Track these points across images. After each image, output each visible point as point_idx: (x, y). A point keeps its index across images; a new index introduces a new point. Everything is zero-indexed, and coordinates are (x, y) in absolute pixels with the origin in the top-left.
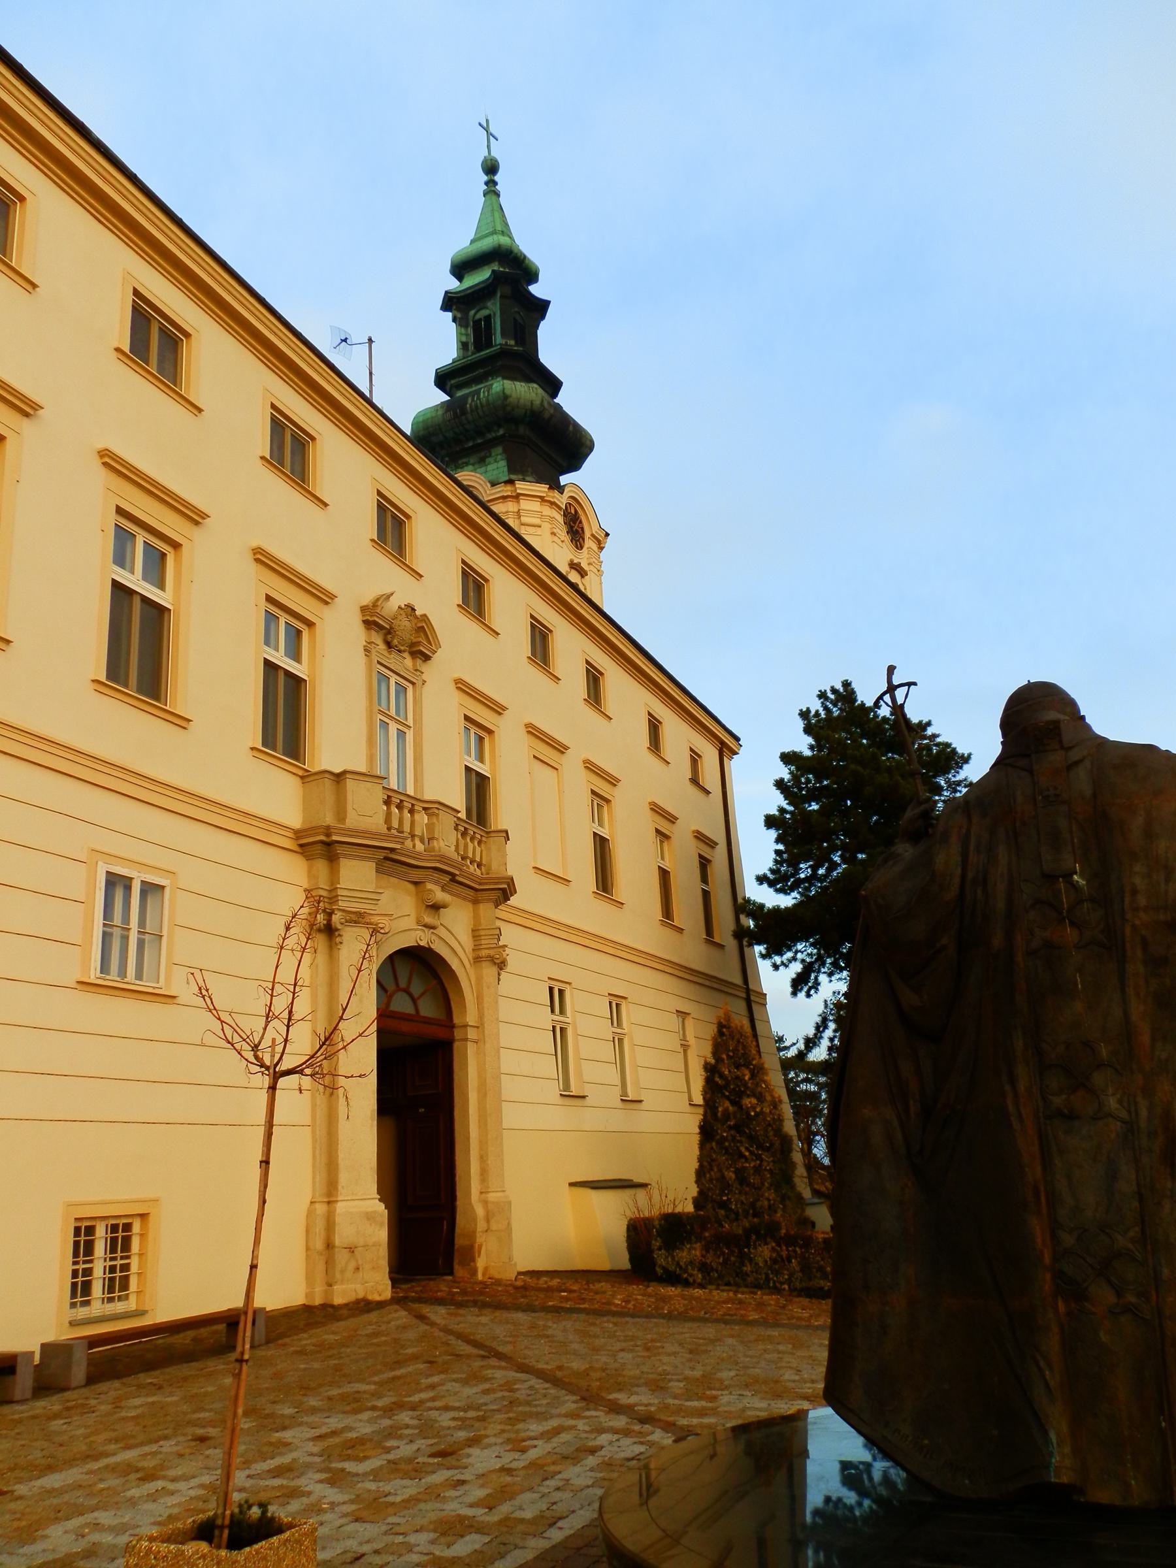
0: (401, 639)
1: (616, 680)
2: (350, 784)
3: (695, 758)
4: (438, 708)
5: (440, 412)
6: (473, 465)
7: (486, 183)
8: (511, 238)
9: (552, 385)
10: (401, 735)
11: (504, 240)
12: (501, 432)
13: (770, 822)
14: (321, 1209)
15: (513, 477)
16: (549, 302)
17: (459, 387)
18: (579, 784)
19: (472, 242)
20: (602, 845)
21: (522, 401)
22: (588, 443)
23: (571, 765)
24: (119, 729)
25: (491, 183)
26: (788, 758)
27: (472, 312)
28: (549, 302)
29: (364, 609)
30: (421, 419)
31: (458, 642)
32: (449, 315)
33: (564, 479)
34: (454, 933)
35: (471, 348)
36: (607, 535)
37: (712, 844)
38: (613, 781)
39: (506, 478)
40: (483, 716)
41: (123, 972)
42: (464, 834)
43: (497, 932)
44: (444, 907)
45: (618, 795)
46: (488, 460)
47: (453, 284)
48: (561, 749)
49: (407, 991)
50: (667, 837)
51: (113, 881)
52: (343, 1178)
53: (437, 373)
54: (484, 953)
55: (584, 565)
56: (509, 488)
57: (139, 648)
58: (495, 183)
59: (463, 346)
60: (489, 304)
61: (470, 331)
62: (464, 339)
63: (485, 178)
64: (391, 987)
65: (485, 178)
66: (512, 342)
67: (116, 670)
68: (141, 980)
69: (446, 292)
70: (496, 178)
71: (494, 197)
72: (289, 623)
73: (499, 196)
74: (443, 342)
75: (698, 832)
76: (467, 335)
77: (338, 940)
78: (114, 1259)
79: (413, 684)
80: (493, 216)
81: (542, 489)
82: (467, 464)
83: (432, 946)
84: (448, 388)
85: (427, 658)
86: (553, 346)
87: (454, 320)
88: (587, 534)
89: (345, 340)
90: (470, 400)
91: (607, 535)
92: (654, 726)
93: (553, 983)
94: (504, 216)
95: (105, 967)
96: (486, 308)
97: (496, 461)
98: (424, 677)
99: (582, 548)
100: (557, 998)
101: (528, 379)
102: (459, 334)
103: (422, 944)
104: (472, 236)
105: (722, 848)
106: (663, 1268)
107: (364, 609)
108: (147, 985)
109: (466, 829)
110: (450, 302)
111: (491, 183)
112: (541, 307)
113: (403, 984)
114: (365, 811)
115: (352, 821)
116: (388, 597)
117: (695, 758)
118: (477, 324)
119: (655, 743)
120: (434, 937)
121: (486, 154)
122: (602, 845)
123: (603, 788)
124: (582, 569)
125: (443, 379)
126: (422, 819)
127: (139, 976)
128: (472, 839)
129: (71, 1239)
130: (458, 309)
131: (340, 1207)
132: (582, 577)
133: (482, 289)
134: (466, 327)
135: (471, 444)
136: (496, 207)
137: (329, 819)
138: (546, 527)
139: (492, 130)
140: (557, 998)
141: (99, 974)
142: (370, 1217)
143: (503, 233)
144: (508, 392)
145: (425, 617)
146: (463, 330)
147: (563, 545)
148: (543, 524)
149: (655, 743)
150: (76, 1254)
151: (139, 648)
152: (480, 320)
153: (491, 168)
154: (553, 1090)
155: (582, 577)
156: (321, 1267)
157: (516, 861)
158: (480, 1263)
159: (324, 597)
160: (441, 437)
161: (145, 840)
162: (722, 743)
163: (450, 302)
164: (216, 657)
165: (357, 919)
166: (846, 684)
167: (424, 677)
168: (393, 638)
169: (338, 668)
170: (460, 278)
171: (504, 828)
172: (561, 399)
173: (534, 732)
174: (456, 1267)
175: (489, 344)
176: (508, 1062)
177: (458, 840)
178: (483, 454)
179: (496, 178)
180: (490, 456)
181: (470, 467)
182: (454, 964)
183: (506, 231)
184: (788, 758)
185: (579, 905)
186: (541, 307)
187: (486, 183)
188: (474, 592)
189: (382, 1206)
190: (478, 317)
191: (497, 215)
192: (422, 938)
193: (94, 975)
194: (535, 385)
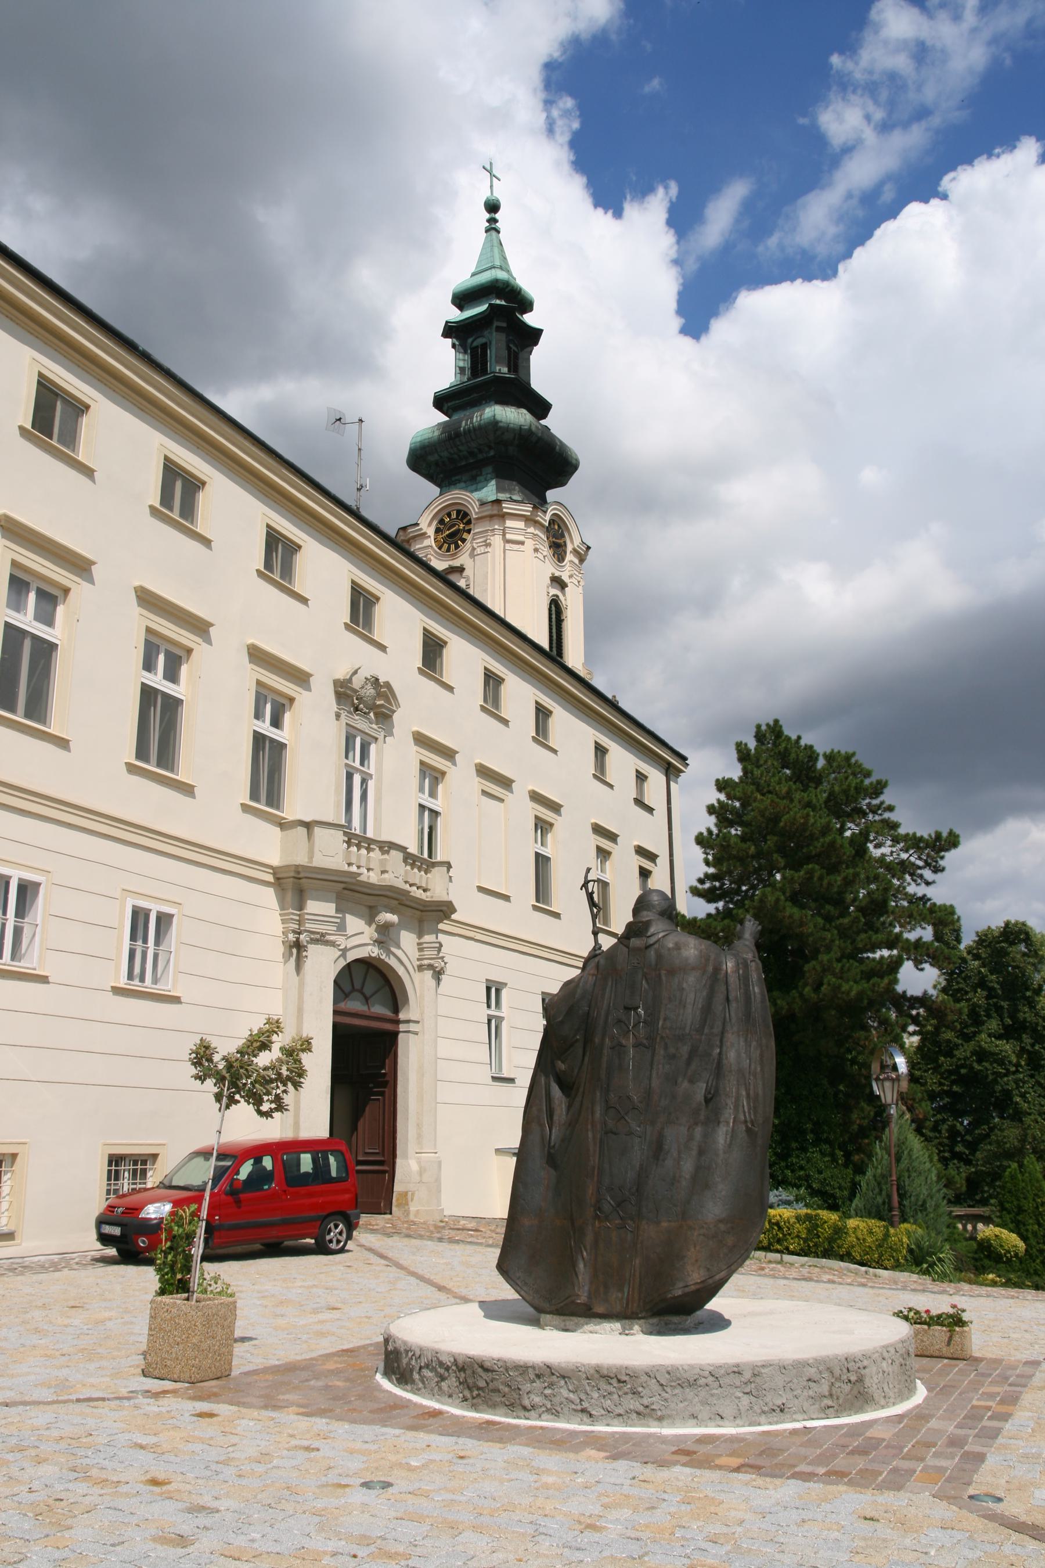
0: (367, 705)
1: (563, 720)
2: (317, 831)
4: (395, 759)
5: (437, 433)
6: (465, 482)
7: (488, 221)
8: (508, 271)
9: (540, 407)
10: (364, 781)
11: (501, 275)
12: (492, 453)
13: (700, 840)
15: (502, 496)
16: (541, 331)
19: (473, 275)
20: (542, 862)
22: (574, 462)
24: (145, 801)
25: (492, 221)
26: (722, 785)
27: (470, 340)
28: (541, 331)
29: (336, 683)
30: (419, 439)
31: (419, 705)
32: (449, 341)
33: (551, 495)
35: (468, 372)
36: (589, 548)
37: (652, 857)
38: (555, 808)
39: (494, 498)
40: (438, 762)
41: (142, 979)
43: (437, 945)
45: (560, 823)
47: (455, 315)
49: (361, 991)
50: (609, 853)
51: (139, 917)
53: (435, 397)
54: (426, 962)
55: (565, 578)
56: (496, 507)
58: (495, 221)
60: (486, 333)
62: (461, 364)
63: (487, 216)
64: (347, 988)
65: (487, 216)
66: (505, 370)
69: (447, 322)
70: (497, 216)
71: (494, 233)
73: (498, 232)
74: (444, 366)
75: (639, 847)
77: (304, 954)
78: (135, 1184)
80: (492, 251)
81: (526, 509)
82: (459, 481)
84: (445, 408)
86: (543, 369)
87: (454, 346)
88: (569, 547)
89: (340, 419)
90: (464, 423)
91: (589, 548)
92: (600, 751)
94: (502, 251)
95: (130, 976)
96: (483, 336)
99: (563, 560)
100: (493, 991)
101: (519, 404)
103: (373, 955)
104: (473, 270)
105: (663, 861)
107: (336, 683)
108: (161, 988)
110: (450, 330)
111: (492, 221)
112: (534, 335)
113: (357, 986)
119: (600, 774)
121: (489, 194)
122: (542, 862)
123: (547, 815)
124: (563, 581)
125: (442, 401)
126: (376, 854)
127: (155, 981)
129: (106, 1168)
130: (457, 338)
133: (479, 320)
134: (465, 352)
135: (463, 463)
136: (495, 243)
137: (301, 859)
138: (530, 544)
139: (494, 172)
140: (493, 991)
141: (126, 980)
143: (501, 268)
144: (498, 418)
145: (387, 685)
146: (461, 356)
149: (600, 774)
150: (109, 1179)
152: (477, 347)
153: (493, 207)
154: (485, 1074)
157: (454, 888)
158: (413, 1208)
159: (301, 678)
161: (159, 881)
162: (669, 764)
163: (450, 330)
165: (321, 939)
166: (776, 721)
169: (313, 731)
170: (461, 308)
171: (445, 859)
172: (550, 422)
173: (484, 772)
174: (394, 1209)
175: (484, 371)
176: (444, 1048)
178: (474, 472)
179: (497, 216)
180: (481, 475)
181: (463, 485)
182: (401, 971)
183: (504, 267)
184: (722, 785)
185: (518, 917)
186: (534, 335)
187: (488, 221)
190: (475, 344)
191: (496, 250)
193: (123, 982)
194: (524, 411)
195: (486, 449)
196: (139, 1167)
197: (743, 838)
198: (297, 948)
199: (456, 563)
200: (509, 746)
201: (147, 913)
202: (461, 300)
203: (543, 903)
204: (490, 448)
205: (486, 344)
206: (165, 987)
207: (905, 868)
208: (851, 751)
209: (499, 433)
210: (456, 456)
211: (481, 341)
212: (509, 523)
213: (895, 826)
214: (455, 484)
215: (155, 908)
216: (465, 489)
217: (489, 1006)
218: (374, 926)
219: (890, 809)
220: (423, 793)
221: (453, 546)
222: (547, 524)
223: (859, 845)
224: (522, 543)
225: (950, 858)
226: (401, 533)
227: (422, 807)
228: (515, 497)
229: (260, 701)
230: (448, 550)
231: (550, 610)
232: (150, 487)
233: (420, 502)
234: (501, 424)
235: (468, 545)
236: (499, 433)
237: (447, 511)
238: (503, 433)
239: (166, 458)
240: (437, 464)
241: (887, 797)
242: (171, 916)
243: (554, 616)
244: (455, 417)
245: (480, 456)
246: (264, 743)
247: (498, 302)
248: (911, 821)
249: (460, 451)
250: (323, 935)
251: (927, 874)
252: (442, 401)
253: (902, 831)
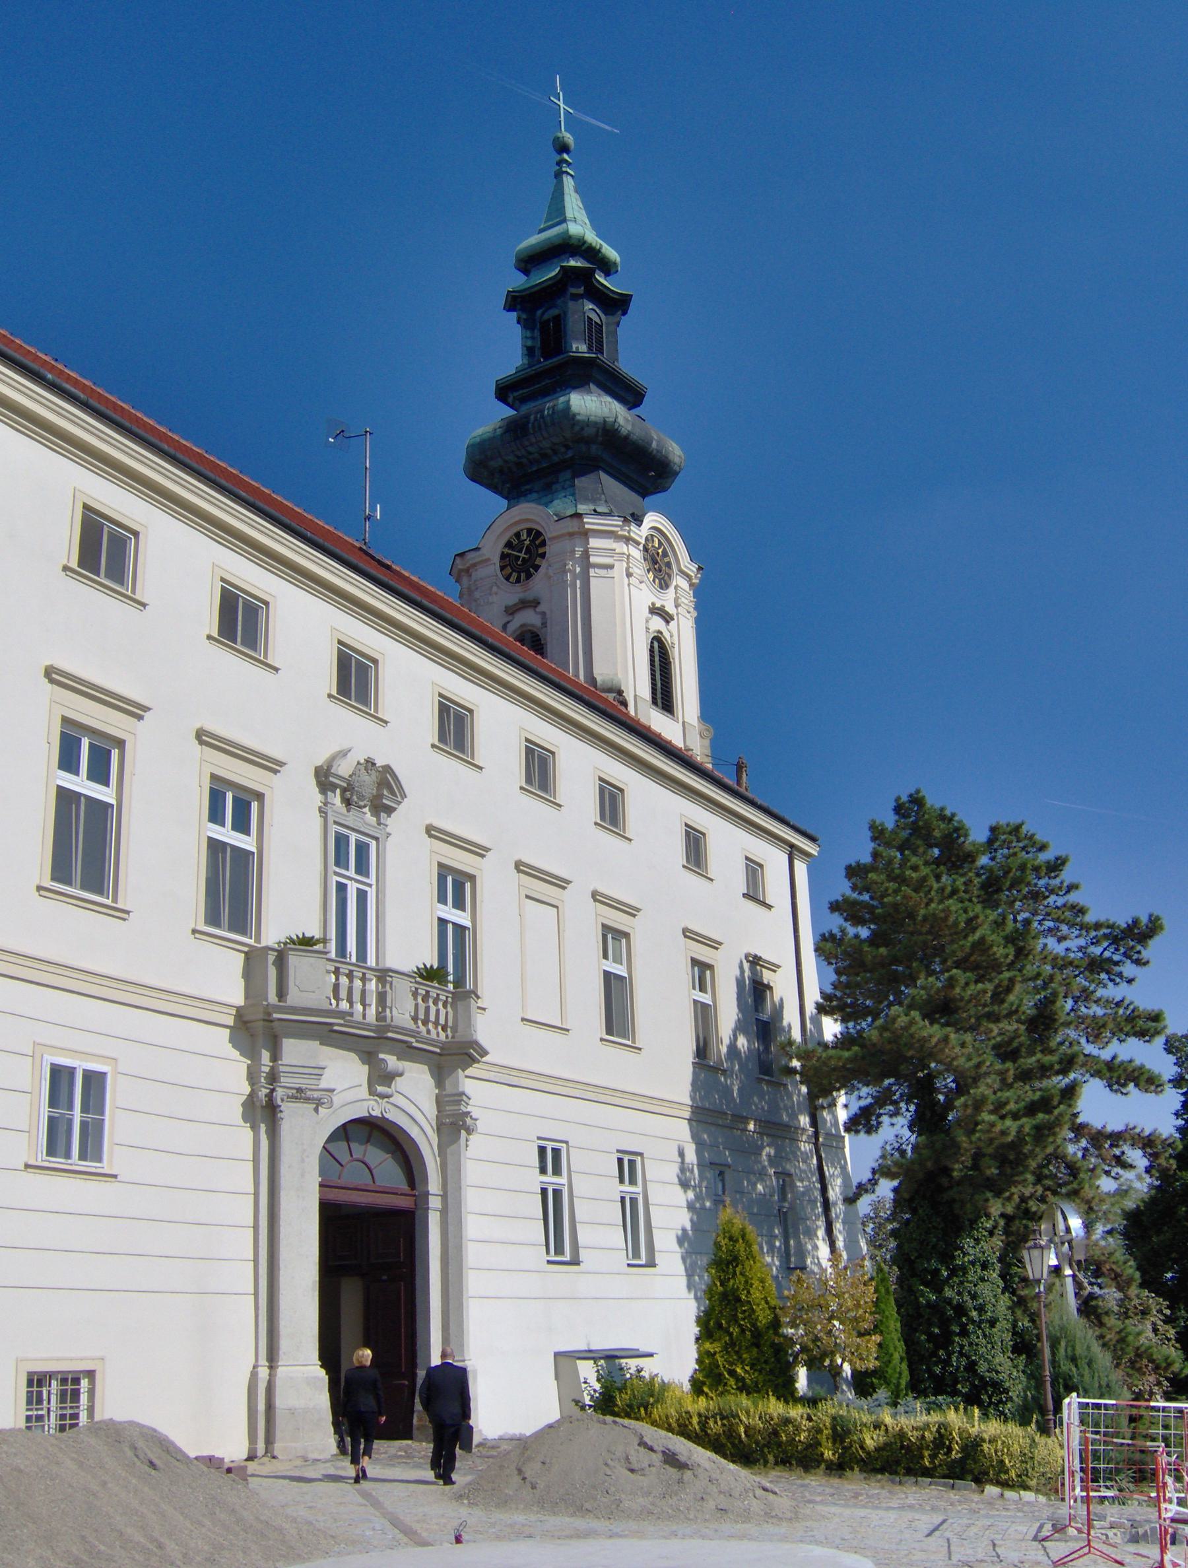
3: (754, 869)
12: (570, 454)
14: (264, 1372)
17: (524, 400)
18: (585, 921)
21: (592, 418)
23: (576, 901)
27: (539, 312)
34: (413, 1099)
35: (538, 352)
42: (425, 998)
44: (401, 1075)
46: (554, 487)
47: (518, 281)
48: (561, 883)
51: (60, 1077)
52: (284, 1344)
55: (670, 608)
56: (575, 521)
57: (84, 849)
59: (530, 351)
60: (559, 302)
61: (537, 333)
62: (529, 343)
67: (61, 870)
68: (85, 1160)
72: (233, 804)
76: (533, 338)
79: (377, 839)
82: (530, 491)
83: (386, 1116)
84: (510, 400)
85: (390, 810)
93: (543, 1143)
97: (564, 488)
98: (388, 830)
99: (667, 587)
102: (525, 338)
103: (374, 1113)
106: (747, 1429)
109: (428, 992)
110: (515, 302)
114: (311, 983)
115: (294, 997)
116: (344, 754)
117: (754, 869)
118: (544, 326)
120: (389, 1106)
123: (619, 920)
124: (667, 613)
125: (504, 392)
128: (435, 1003)
130: (523, 310)
131: (281, 1371)
132: (668, 622)
134: (532, 329)
135: (535, 469)
140: (550, 1158)
142: (311, 1381)
145: (388, 769)
146: (529, 334)
147: (643, 586)
148: (617, 564)
151: (84, 849)
152: (548, 321)
155: (668, 622)
156: (453, 1338)
159: (272, 765)
160: (500, 462)
161: (85, 1034)
162: (792, 846)
163: (515, 302)
164: (163, 840)
167: (388, 830)
168: (352, 795)
170: (526, 272)
177: (417, 1005)
180: (557, 482)
181: (535, 495)
182: (414, 1132)
185: (587, 1052)
188: (454, 728)
189: (323, 1372)
190: (546, 317)
192: (375, 1108)
195: (563, 450)
196: (35, 1389)
197: (874, 941)
198: (264, 1112)
199: (529, 595)
200: (564, 832)
201: (71, 1071)
202: (529, 262)
203: (618, 1036)
204: (567, 447)
205: (559, 316)
206: (105, 1167)
207: (1096, 966)
208: (1019, 821)
209: (577, 428)
210: (524, 461)
211: (555, 312)
212: (594, 542)
213: (1082, 911)
214: (525, 495)
215: (81, 1065)
216: (538, 501)
217: (622, 1181)
218: (1168, 1087)
219: (1071, 888)
220: (446, 904)
221: (523, 576)
222: (643, 542)
223: (1019, 941)
224: (611, 567)
225: (1152, 950)
226: (458, 560)
227: (442, 922)
228: (599, 509)
229: (216, 799)
230: (518, 581)
231: (652, 651)
232: (65, 542)
233: (490, 518)
234: (578, 417)
235: (542, 570)
236: (577, 428)
237: (515, 530)
238: (582, 429)
239: (86, 507)
240: (501, 472)
241: (1067, 875)
242: (103, 1075)
243: (657, 659)
244: (525, 409)
245: (556, 459)
246: (224, 852)
247: (572, 263)
248: (1108, 903)
249: (530, 453)
250: (299, 1090)
251: (1128, 969)
252: (504, 392)
253: (1090, 918)
